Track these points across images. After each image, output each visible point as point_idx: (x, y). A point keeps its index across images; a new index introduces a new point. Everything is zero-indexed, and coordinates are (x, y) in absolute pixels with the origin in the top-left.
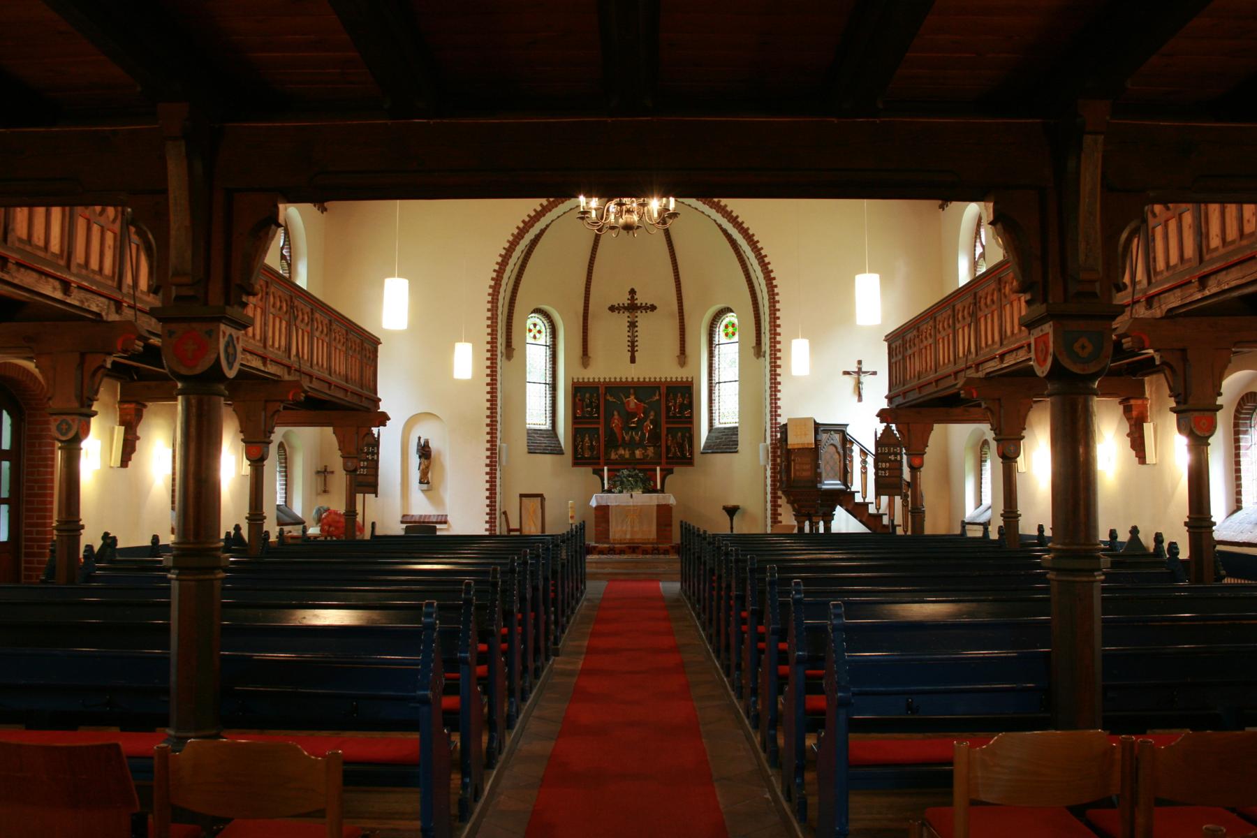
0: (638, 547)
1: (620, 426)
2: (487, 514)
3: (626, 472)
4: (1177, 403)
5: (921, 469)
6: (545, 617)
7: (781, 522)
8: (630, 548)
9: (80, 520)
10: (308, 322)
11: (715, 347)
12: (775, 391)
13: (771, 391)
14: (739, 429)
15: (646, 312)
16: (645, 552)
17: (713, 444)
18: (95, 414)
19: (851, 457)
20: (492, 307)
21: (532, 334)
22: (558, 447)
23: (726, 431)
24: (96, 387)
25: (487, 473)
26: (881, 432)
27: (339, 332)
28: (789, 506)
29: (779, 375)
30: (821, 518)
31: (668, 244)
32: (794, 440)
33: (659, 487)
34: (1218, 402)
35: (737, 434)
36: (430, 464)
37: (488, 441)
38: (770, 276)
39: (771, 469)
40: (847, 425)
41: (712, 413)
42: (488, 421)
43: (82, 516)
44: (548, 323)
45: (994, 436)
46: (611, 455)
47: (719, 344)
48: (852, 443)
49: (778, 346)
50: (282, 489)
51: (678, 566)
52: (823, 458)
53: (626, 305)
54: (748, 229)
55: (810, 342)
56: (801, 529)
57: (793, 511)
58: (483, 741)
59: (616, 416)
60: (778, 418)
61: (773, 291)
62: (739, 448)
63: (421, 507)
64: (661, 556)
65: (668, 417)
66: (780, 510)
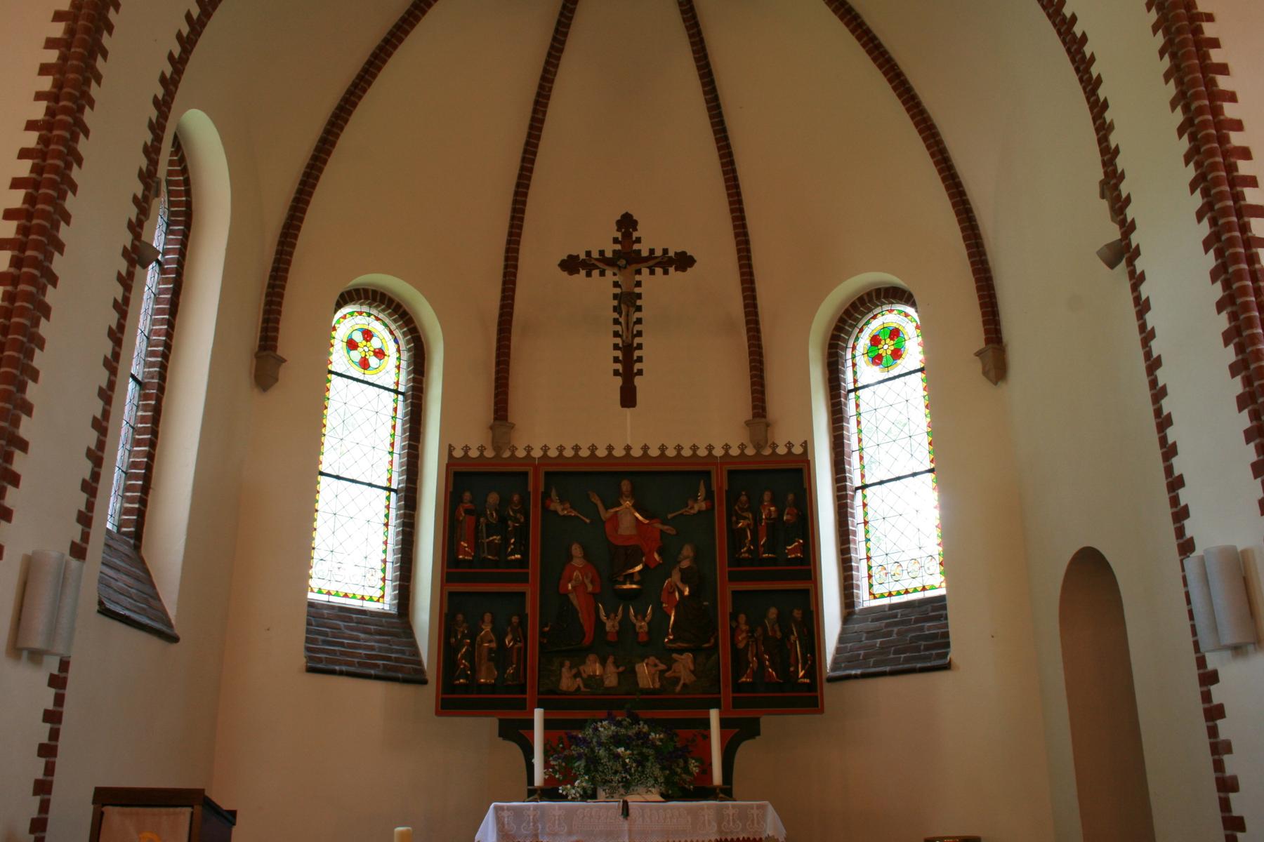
1: (590, 588)
3: (606, 729)
11: (846, 397)
14: (949, 603)
22: (407, 662)
33: (717, 777)
41: (851, 568)
44: (404, 334)
46: (559, 681)
47: (856, 390)
53: (609, 254)
59: (578, 561)
62: (954, 654)
65: (735, 561)
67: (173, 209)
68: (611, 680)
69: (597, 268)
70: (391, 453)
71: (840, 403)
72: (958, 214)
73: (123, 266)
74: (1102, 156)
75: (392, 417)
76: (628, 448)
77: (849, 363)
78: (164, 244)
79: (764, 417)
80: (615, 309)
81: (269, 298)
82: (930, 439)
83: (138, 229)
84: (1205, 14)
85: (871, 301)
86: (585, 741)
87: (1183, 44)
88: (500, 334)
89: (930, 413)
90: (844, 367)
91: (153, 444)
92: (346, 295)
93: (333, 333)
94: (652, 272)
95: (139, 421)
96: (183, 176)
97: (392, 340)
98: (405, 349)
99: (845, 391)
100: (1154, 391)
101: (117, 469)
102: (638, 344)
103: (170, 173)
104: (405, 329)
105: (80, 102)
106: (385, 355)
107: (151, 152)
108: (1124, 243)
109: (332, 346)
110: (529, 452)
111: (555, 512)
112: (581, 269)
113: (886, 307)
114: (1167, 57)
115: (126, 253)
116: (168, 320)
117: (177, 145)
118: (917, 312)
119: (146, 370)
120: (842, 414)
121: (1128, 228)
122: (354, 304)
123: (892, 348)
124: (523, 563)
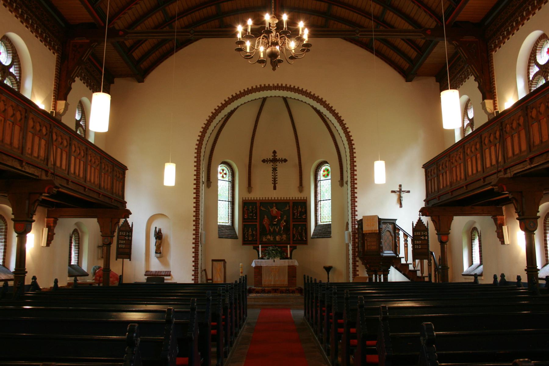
0: (278, 289)
1: (268, 223)
2: (193, 271)
3: (271, 248)
4: (519, 215)
5: (447, 243)
6: (231, 324)
7: (358, 275)
8: (273, 289)
9: (26, 269)
10: (84, 156)
11: (318, 182)
12: (354, 202)
13: (352, 202)
15: (282, 163)
16: (282, 292)
17: (317, 233)
18: (34, 221)
19: (399, 238)
20: (197, 155)
21: (221, 175)
22: (234, 235)
23: (324, 226)
24: (35, 209)
25: (193, 248)
26: (416, 223)
27: (94, 157)
28: (363, 266)
29: (356, 193)
30: (382, 273)
31: (293, 127)
32: (366, 228)
33: (289, 256)
34: (538, 215)
35: (331, 228)
36: (161, 242)
37: (194, 230)
38: (350, 139)
39: (352, 245)
40: (396, 220)
41: (317, 217)
42: (194, 218)
43: (26, 267)
44: (230, 169)
45: (436, 232)
47: (320, 181)
48: (399, 230)
49: (355, 177)
50: (76, 256)
51: (302, 301)
52: (383, 238)
53: (271, 159)
54: (338, 113)
55: (385, 163)
56: (371, 279)
57: (366, 269)
58: (412, 50)
60: (356, 217)
61: (352, 147)
62: (332, 235)
63: (156, 266)
64: (291, 294)
65: (293, 218)
66: (357, 268)
68: (272, 239)
86: (268, 250)
111: (262, 209)
124: (256, 219)
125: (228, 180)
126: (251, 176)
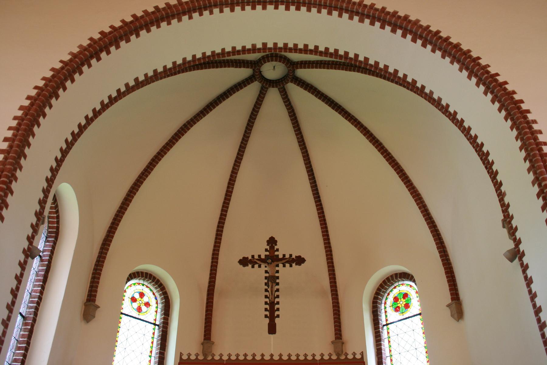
11: (382, 329)
44: (160, 295)
47: (387, 325)
53: (263, 257)
67: (49, 230)
69: (257, 263)
70: (150, 356)
71: (379, 332)
72: (433, 236)
73: (22, 258)
74: (501, 207)
75: (149, 356)
76: (272, 355)
77: (383, 311)
78: (44, 247)
79: (341, 339)
80: (266, 284)
81: (94, 275)
82: (426, 350)
83: (32, 240)
84: (543, 142)
85: (393, 280)
87: (534, 156)
88: (209, 295)
89: (426, 336)
90: (381, 313)
91: (26, 349)
92: (132, 275)
93: (125, 294)
94: (284, 266)
95: (21, 337)
96: (56, 214)
97: (154, 298)
98: (160, 302)
99: (381, 325)
100: (539, 324)
101: (6, 362)
102: (277, 302)
103: (50, 213)
104: (161, 292)
105: (11, 179)
106: (150, 305)
107: (42, 203)
108: (516, 250)
109: (124, 300)
110: (221, 357)
112: (249, 264)
113: (401, 283)
114: (527, 161)
115: (24, 251)
116: (54, 240)
117: (55, 199)
118: (416, 284)
119: (28, 310)
120: (380, 337)
121: (518, 242)
122: (136, 279)
123: (404, 303)
125: (153, 322)
126: (211, 315)
